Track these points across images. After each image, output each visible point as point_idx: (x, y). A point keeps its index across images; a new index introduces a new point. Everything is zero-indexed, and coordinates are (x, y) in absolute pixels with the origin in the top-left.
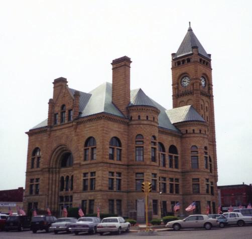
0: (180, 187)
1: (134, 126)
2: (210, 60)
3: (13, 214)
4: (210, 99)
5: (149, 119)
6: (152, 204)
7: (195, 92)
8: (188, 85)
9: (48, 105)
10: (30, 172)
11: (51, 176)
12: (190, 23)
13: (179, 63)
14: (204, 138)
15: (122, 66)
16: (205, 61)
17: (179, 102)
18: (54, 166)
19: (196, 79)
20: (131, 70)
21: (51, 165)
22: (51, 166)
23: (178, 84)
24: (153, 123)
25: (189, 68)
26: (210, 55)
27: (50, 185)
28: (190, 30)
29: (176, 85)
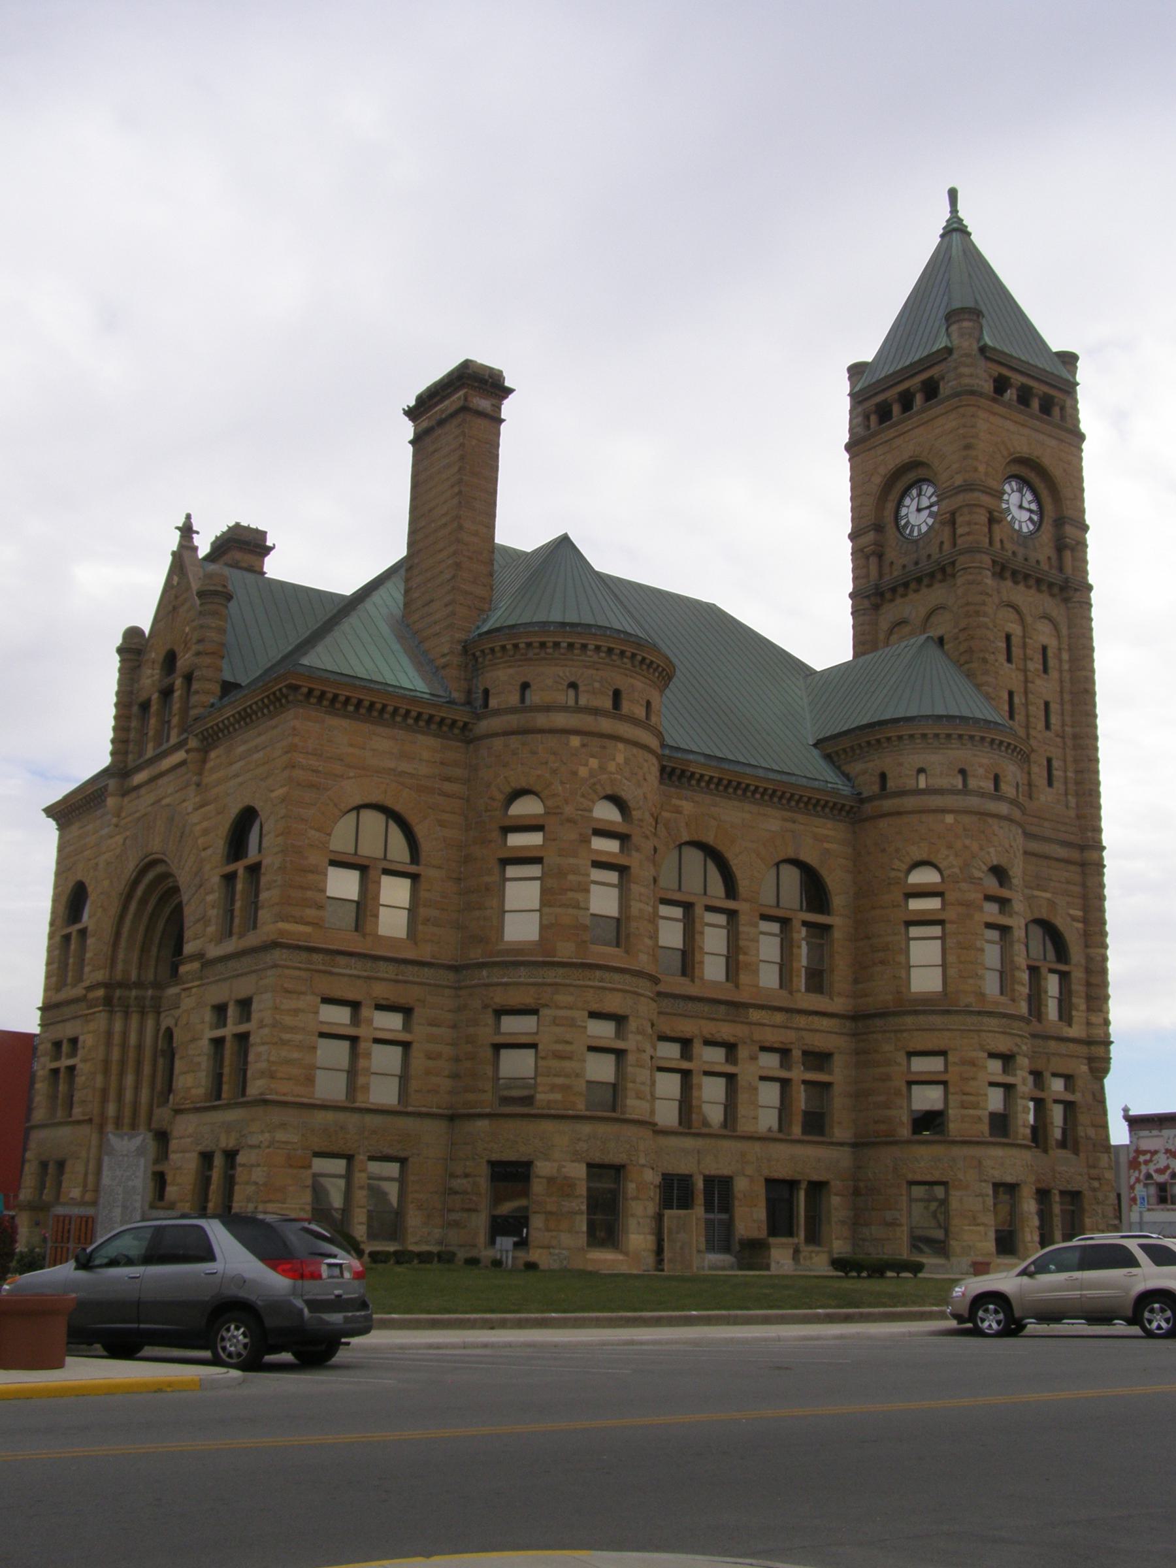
0: (839, 1103)
1: (498, 743)
2: (1069, 388)
3: (958, 1291)
4: (1066, 600)
5: (626, 707)
6: (582, 1189)
7: (962, 560)
8: (931, 528)
9: (115, 661)
10: (57, 1006)
11: (118, 1026)
12: (953, 194)
13: (884, 413)
14: (983, 814)
15: (459, 416)
16: (1042, 391)
17: (884, 626)
18: (134, 976)
19: (968, 487)
20: (508, 435)
21: (120, 966)
22: (118, 976)
23: (879, 528)
24: (606, 725)
25: (926, 435)
26: (1069, 359)
27: (114, 1069)
28: (955, 230)
29: (871, 536)
